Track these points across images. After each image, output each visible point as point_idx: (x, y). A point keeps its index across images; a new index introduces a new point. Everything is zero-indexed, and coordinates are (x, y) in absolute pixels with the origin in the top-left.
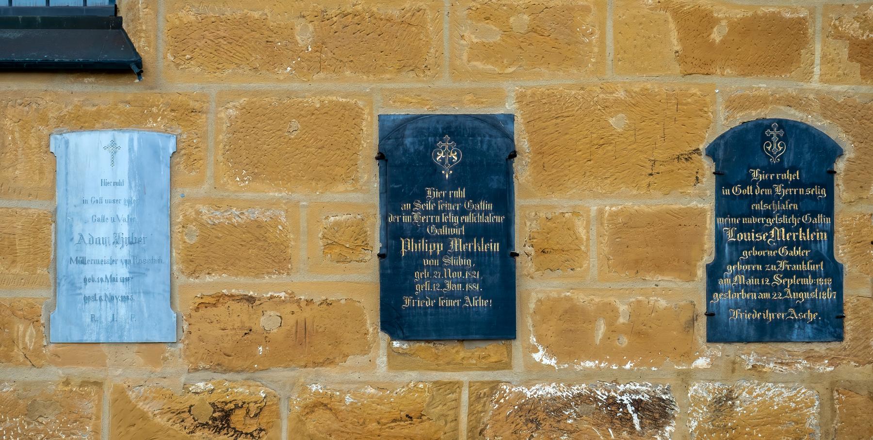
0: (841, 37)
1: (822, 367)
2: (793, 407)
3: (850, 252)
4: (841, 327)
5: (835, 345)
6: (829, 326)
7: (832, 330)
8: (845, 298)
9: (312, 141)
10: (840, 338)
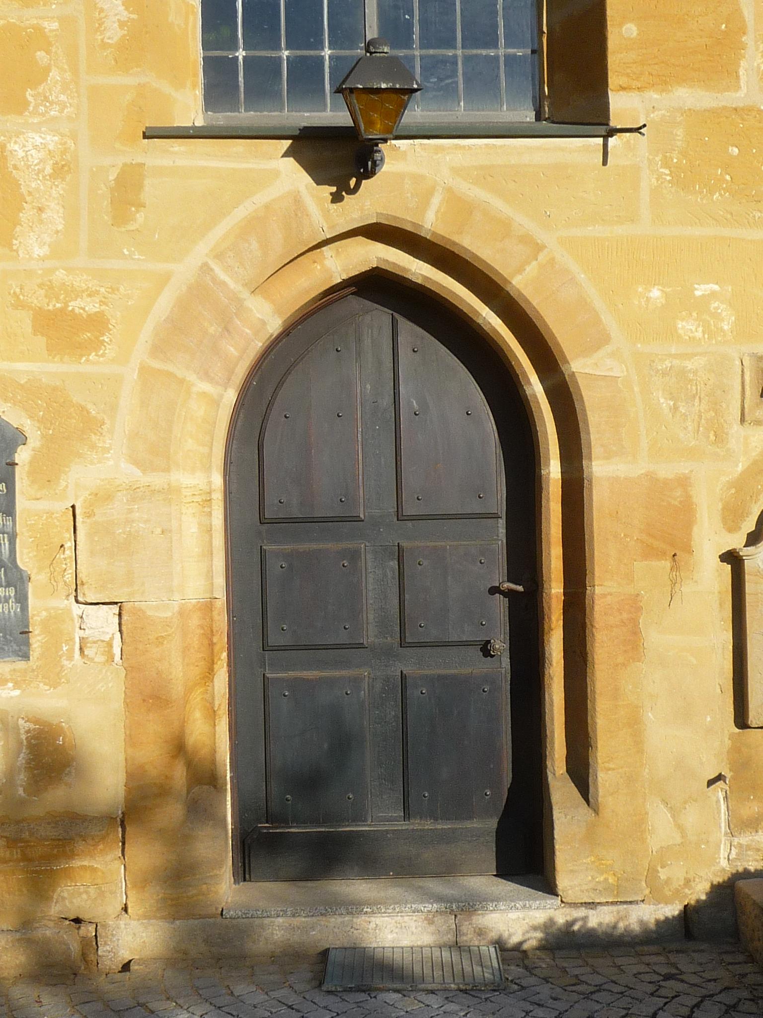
0: (23, 307)
1: (6, 691)
2: (465, 938)
3: (35, 556)
4: (27, 644)
5: (21, 665)
6: (12, 644)
7: (15, 647)
8: (31, 610)
9: (271, 977)
10: (26, 657)
